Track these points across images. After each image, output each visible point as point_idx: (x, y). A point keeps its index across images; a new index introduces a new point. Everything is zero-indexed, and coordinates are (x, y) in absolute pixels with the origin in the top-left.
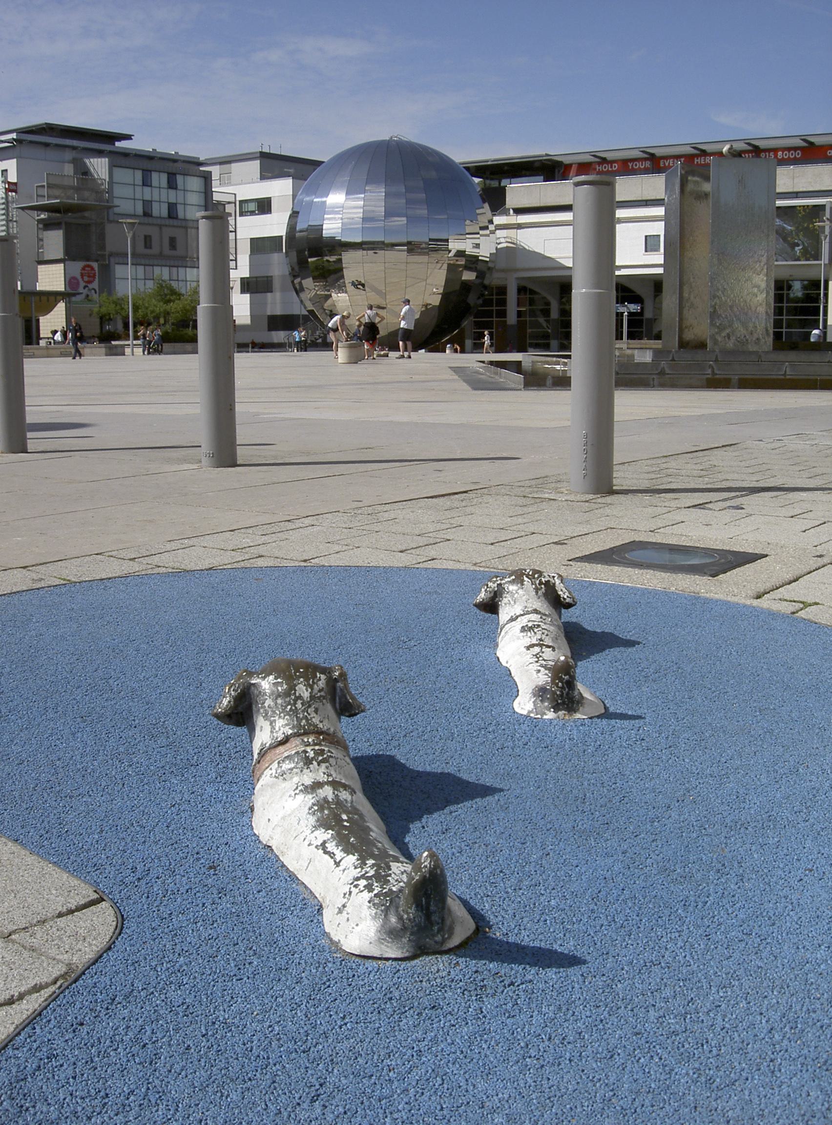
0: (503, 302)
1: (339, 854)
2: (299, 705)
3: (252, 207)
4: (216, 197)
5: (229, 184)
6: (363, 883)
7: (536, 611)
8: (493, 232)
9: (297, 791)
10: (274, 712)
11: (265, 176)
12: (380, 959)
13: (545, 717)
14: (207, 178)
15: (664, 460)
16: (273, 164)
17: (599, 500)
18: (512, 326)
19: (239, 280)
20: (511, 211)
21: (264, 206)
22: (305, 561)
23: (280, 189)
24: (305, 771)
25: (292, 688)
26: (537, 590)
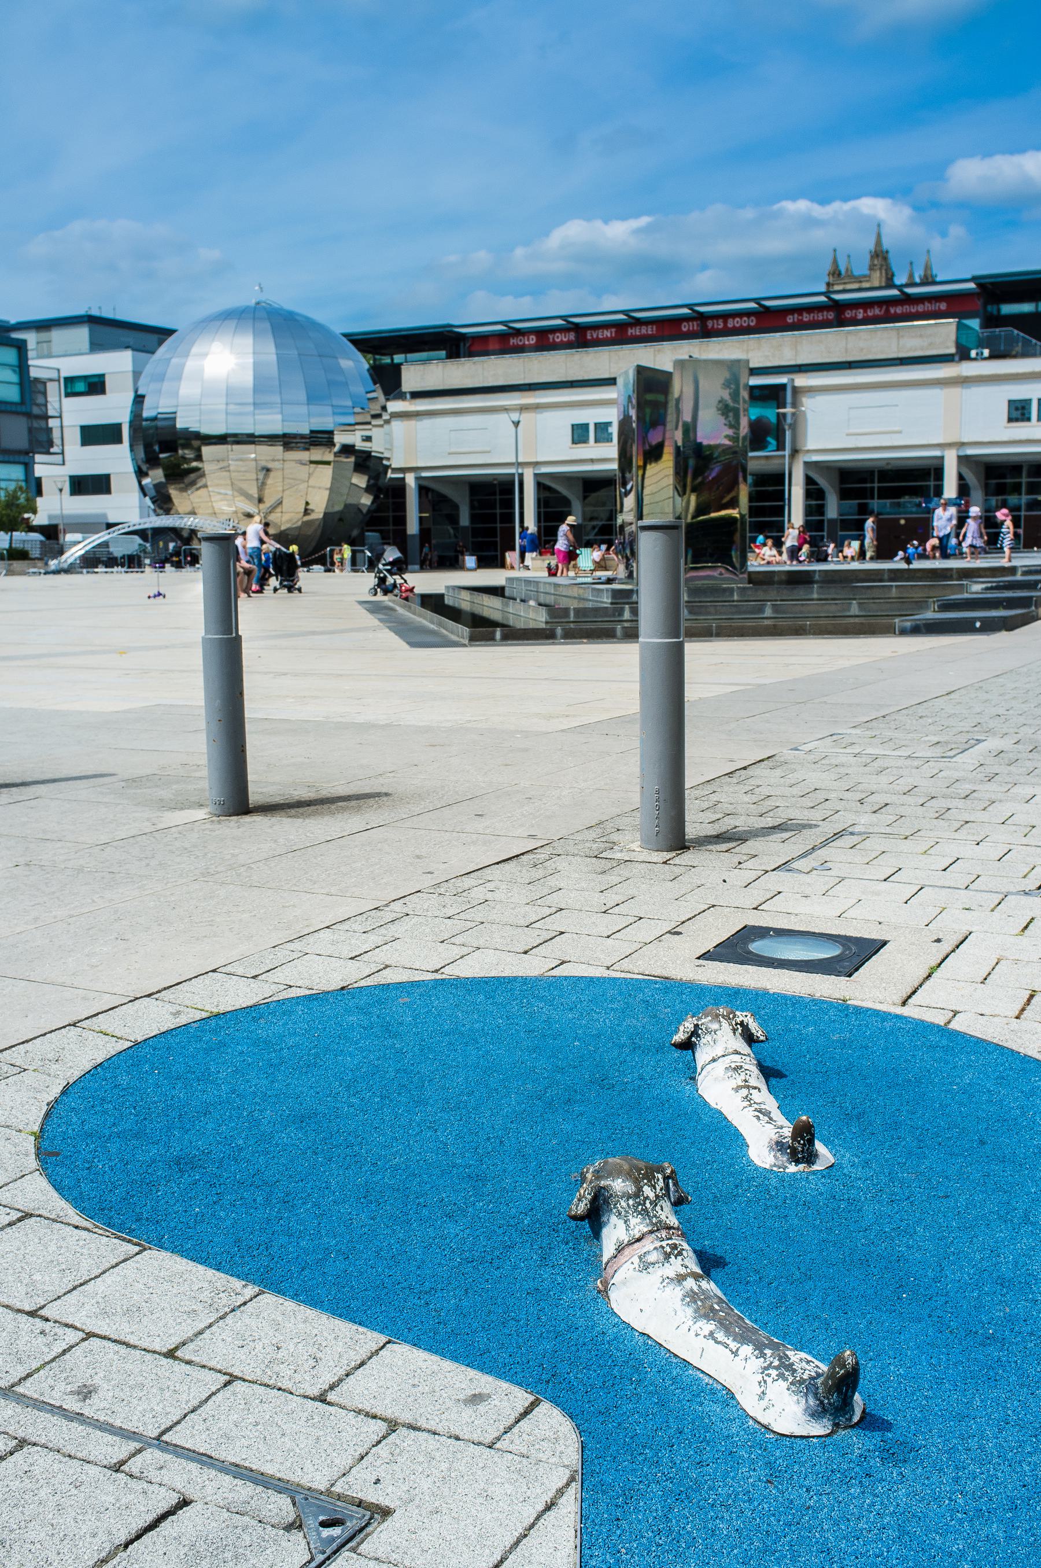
0: (402, 507)
1: (733, 1345)
2: (648, 1205)
3: (81, 387)
4: (34, 373)
5: (50, 356)
6: (774, 1373)
7: (737, 1053)
8: (387, 422)
9: (664, 1284)
10: (627, 1212)
11: (97, 346)
12: (791, 1436)
13: (787, 1171)
14: (21, 347)
15: (709, 788)
16: (107, 331)
17: (677, 861)
18: (413, 536)
19: (68, 479)
20: (408, 396)
21: (96, 386)
22: (436, 971)
23: (115, 364)
24: (666, 1264)
25: (640, 1189)
26: (734, 1030)
